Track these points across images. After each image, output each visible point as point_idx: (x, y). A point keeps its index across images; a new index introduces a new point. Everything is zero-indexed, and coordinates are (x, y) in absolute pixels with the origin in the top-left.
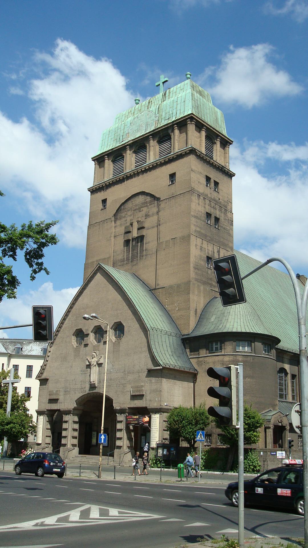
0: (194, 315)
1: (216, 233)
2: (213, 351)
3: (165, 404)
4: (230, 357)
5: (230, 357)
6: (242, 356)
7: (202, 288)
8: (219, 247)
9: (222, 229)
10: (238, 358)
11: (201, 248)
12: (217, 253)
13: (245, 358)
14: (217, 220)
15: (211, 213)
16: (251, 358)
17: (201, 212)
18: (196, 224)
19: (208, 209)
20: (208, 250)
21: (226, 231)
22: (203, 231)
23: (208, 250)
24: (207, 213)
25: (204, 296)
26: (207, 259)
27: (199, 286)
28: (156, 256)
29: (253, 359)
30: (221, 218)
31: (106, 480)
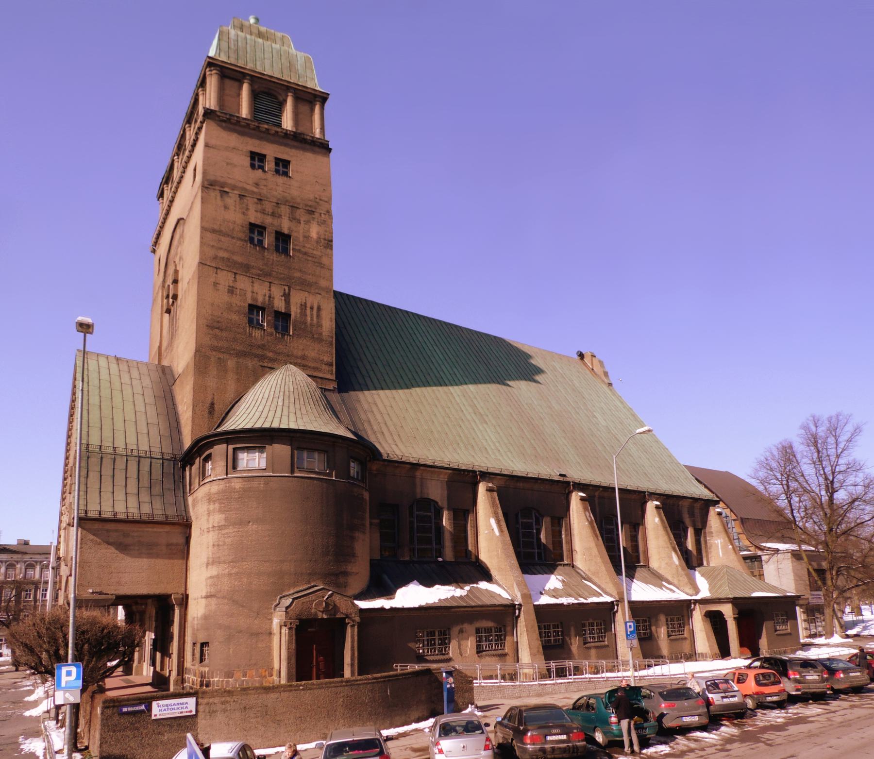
0: (207, 415)
1: (278, 262)
2: (613, 528)
3: (91, 591)
4: (219, 485)
5: (219, 485)
6: (240, 480)
7: (231, 363)
8: (286, 288)
9: (297, 254)
10: (232, 484)
11: (231, 291)
12: (283, 298)
13: (249, 483)
14: (283, 240)
15: (264, 225)
16: (262, 481)
17: (235, 222)
18: (216, 245)
19: (254, 217)
20: (253, 292)
21: (310, 259)
22: (237, 258)
23: (253, 292)
24: (251, 224)
25: (238, 379)
26: (249, 309)
27: (221, 362)
28: (151, 327)
29: (266, 484)
30: (294, 235)
31: (425, 668)
